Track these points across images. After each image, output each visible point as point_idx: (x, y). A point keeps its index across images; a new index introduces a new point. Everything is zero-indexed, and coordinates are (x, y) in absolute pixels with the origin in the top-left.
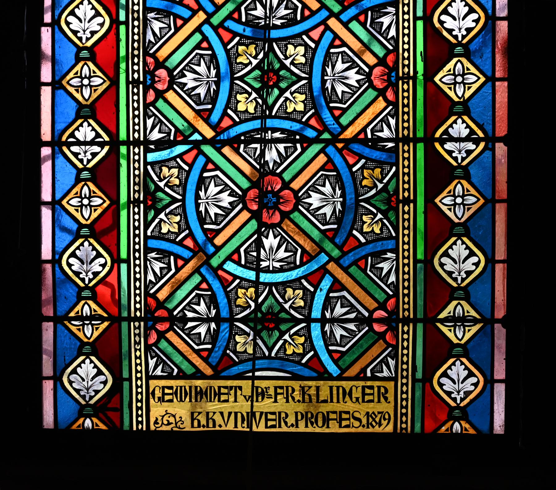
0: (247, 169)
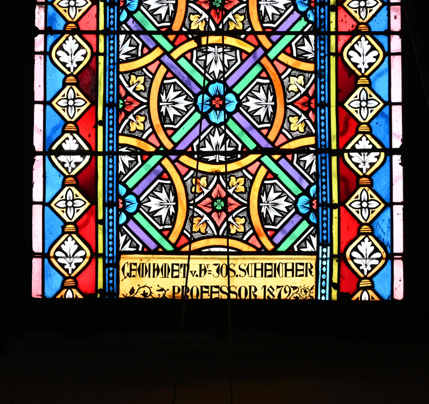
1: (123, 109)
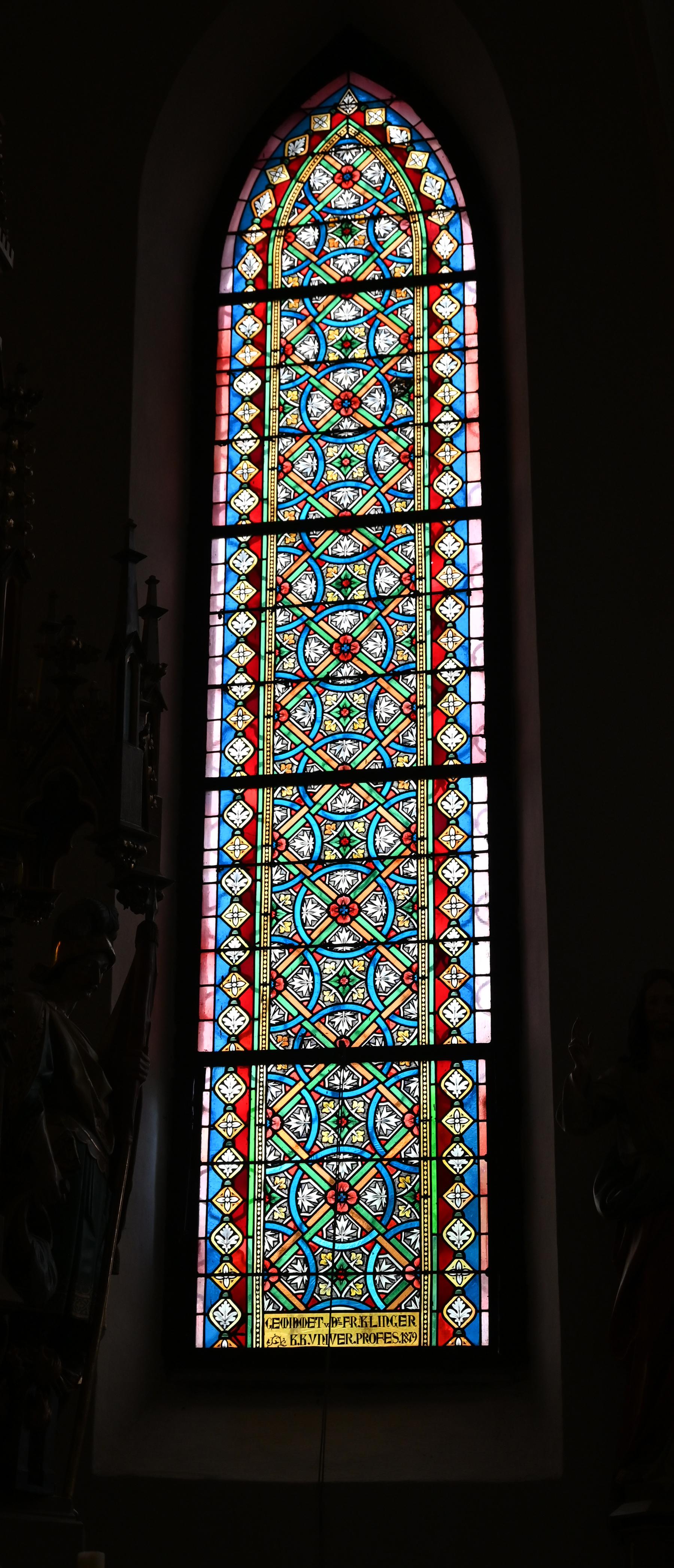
1: (278, 720)
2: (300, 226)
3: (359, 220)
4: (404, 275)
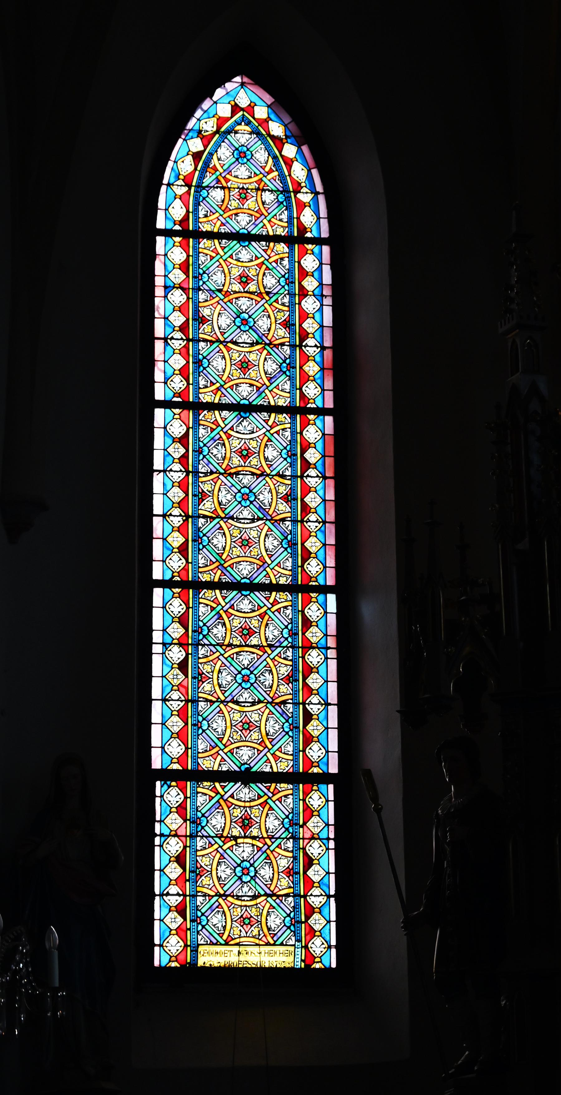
0: (235, 310)
2: (211, 187)
3: (252, 189)
4: (285, 405)
